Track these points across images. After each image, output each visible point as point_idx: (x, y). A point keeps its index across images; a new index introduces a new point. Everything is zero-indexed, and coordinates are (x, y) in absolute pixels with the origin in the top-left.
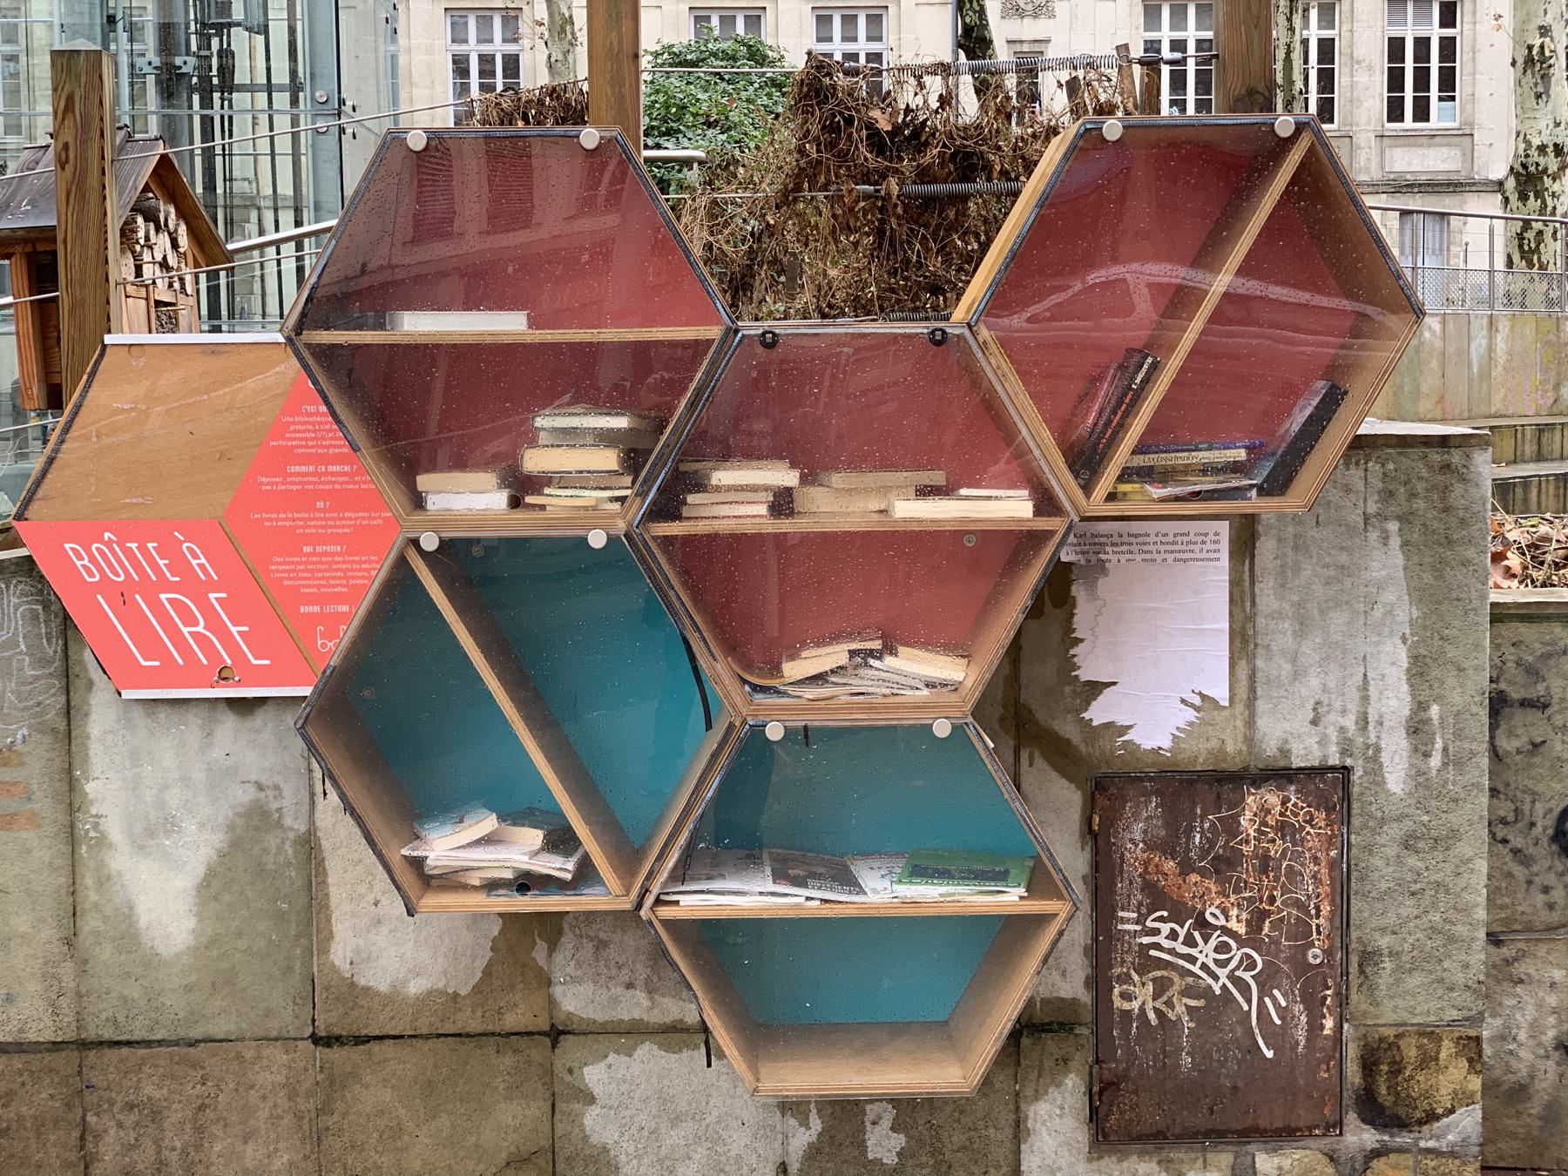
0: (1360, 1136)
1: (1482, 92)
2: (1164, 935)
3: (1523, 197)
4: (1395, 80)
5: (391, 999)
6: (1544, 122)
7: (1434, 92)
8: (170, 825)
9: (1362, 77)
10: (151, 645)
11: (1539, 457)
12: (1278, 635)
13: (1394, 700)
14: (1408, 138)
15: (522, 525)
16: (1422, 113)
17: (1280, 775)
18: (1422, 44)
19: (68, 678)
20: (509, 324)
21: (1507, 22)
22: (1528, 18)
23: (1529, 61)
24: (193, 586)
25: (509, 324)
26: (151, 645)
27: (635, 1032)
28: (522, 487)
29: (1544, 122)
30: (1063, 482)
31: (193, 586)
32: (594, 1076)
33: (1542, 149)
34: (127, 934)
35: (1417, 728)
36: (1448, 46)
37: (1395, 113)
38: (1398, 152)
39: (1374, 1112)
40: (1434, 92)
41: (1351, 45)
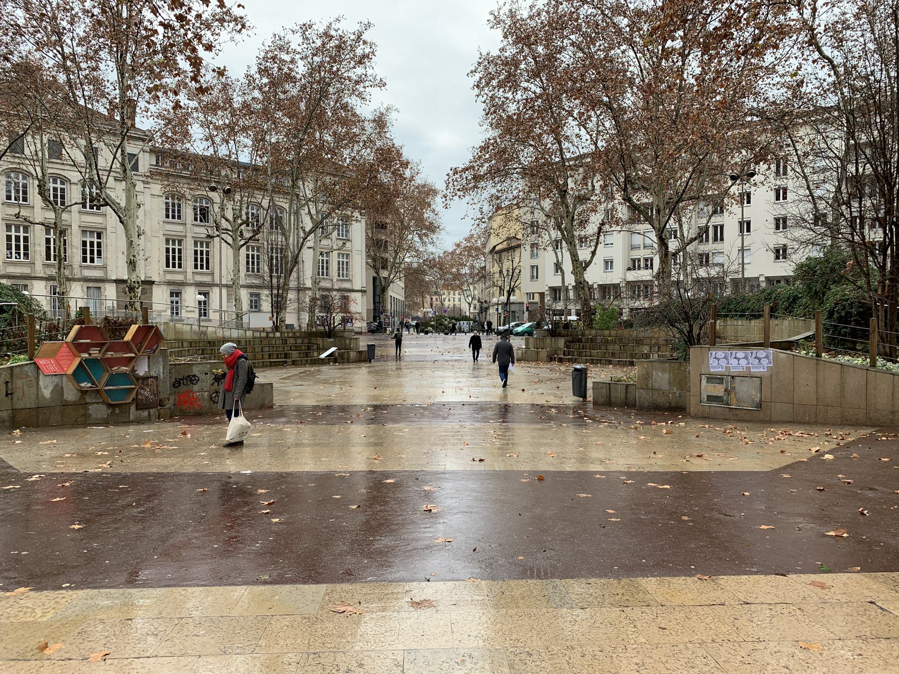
0: (159, 408)
1: (109, 256)
2: (142, 391)
3: (130, 293)
4: (84, 252)
5: (70, 401)
6: (134, 276)
7: (96, 256)
8: (48, 386)
9: (75, 250)
10: (47, 370)
11: (278, 358)
12: (152, 365)
13: (161, 370)
14: (88, 267)
15: (90, 357)
16: (92, 260)
17: (152, 377)
18: (92, 244)
19: (38, 373)
20: (89, 341)
21: (125, 253)
22: (130, 253)
23: (131, 263)
24: (52, 364)
25: (89, 341)
26: (47, 370)
27: (93, 403)
28: (90, 354)
29: (134, 276)
30: (137, 353)
31: (52, 364)
32: (90, 407)
33: (134, 282)
34: (43, 397)
35: (163, 373)
36: (99, 245)
37: (85, 260)
38: (86, 271)
39: (161, 406)
40: (96, 256)
41: (71, 241)
